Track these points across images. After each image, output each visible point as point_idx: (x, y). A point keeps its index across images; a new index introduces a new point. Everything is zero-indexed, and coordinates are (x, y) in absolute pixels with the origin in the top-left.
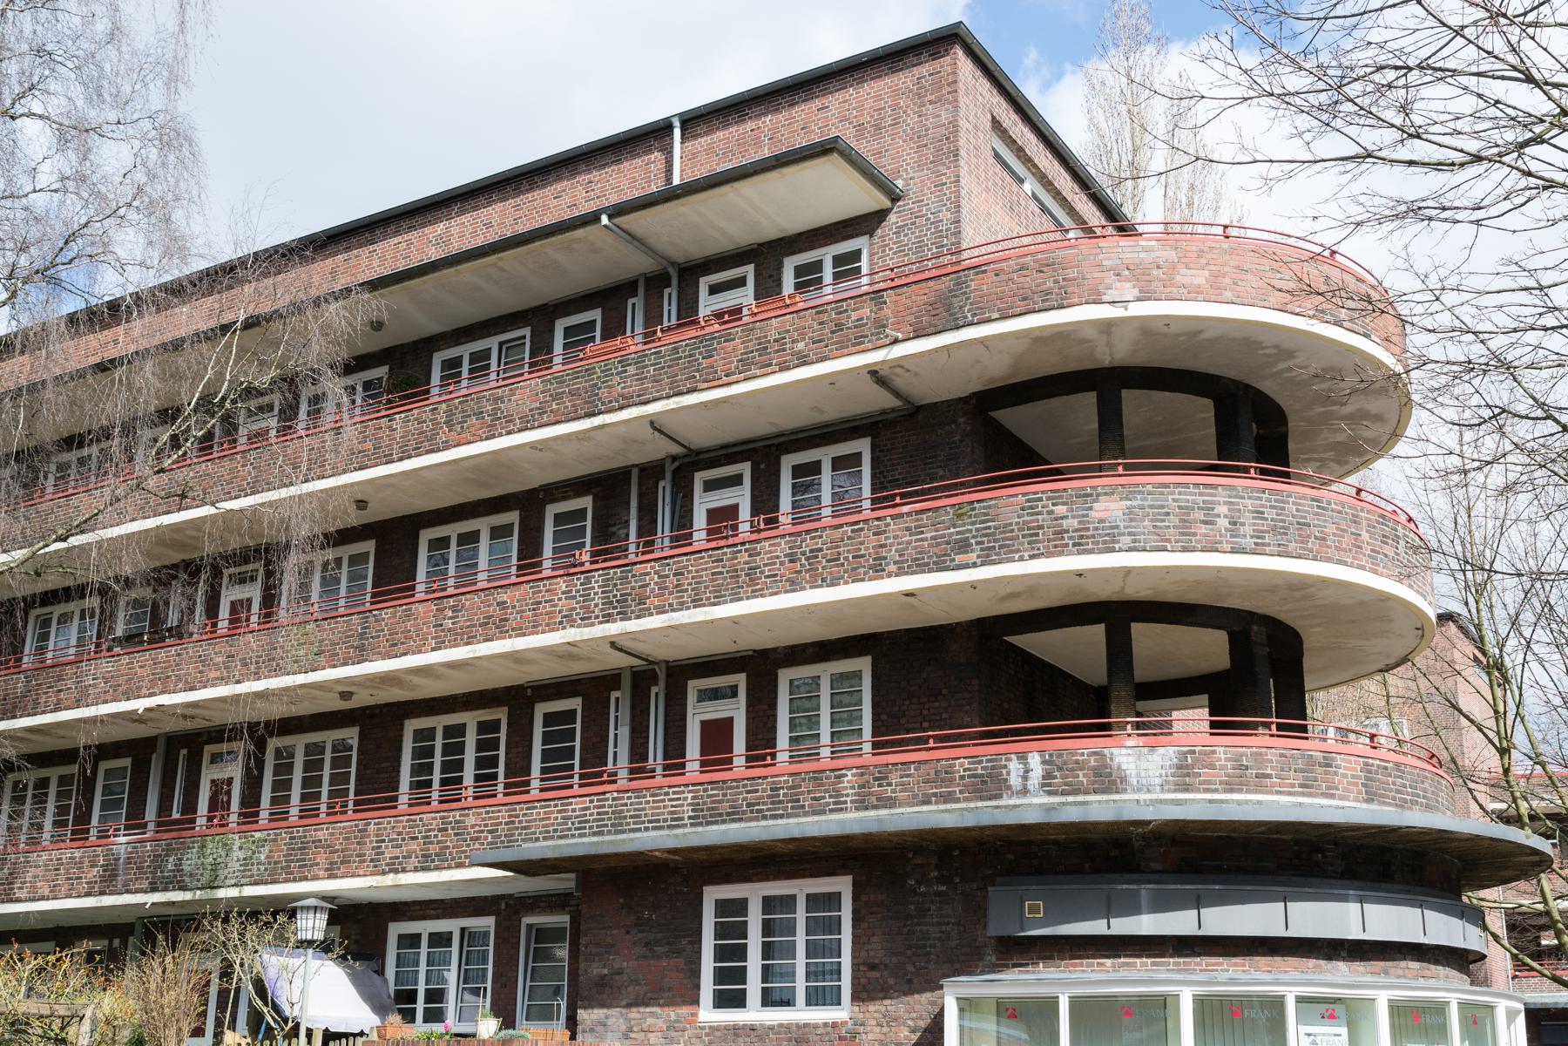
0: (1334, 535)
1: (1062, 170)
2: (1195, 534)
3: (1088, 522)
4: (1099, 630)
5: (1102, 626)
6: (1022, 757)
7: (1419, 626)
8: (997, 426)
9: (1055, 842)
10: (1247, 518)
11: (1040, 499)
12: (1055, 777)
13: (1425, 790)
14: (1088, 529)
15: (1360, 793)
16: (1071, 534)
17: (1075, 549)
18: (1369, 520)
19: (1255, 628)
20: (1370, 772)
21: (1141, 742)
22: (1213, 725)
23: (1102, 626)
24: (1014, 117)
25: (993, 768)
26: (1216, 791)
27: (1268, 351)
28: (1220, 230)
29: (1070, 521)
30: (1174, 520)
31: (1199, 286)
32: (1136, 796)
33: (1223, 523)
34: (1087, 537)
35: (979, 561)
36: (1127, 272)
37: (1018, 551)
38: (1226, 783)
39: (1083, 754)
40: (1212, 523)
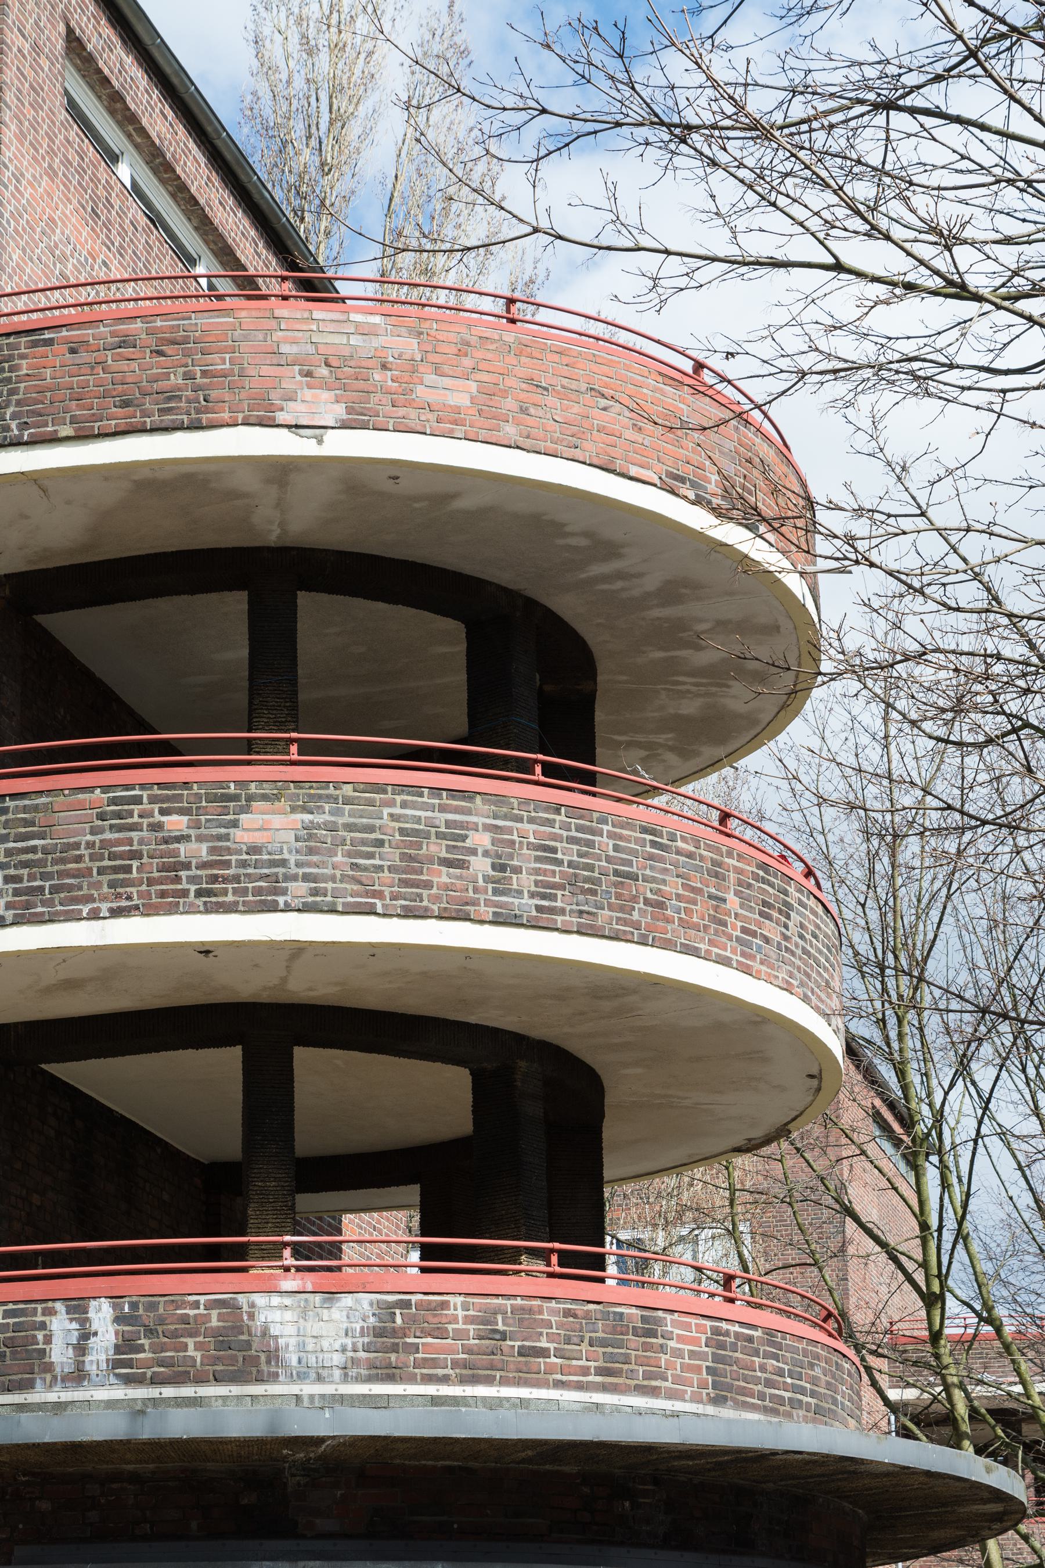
0: (679, 897)
1: (191, 145)
2: (428, 885)
3: (229, 851)
4: (231, 1058)
5: (237, 1051)
6: (78, 1308)
7: (815, 1071)
8: (47, 640)
9: (135, 1478)
10: (525, 859)
11: (138, 800)
12: (141, 1349)
13: (814, 1380)
14: (227, 864)
15: (703, 1385)
16: (194, 872)
17: (199, 902)
18: (739, 871)
19: (523, 1064)
20: (722, 1346)
21: (309, 1281)
22: (428, 1252)
23: (237, 1051)
24: (108, 31)
25: (17, 1328)
26: (445, 1380)
27: (573, 541)
28: (499, 307)
29: (193, 845)
30: (391, 855)
31: (457, 410)
32: (295, 1389)
33: (481, 865)
34: (226, 880)
35: (9, 915)
36: (324, 371)
37: (89, 899)
38: (465, 1365)
39: (196, 1305)
40: (462, 865)
